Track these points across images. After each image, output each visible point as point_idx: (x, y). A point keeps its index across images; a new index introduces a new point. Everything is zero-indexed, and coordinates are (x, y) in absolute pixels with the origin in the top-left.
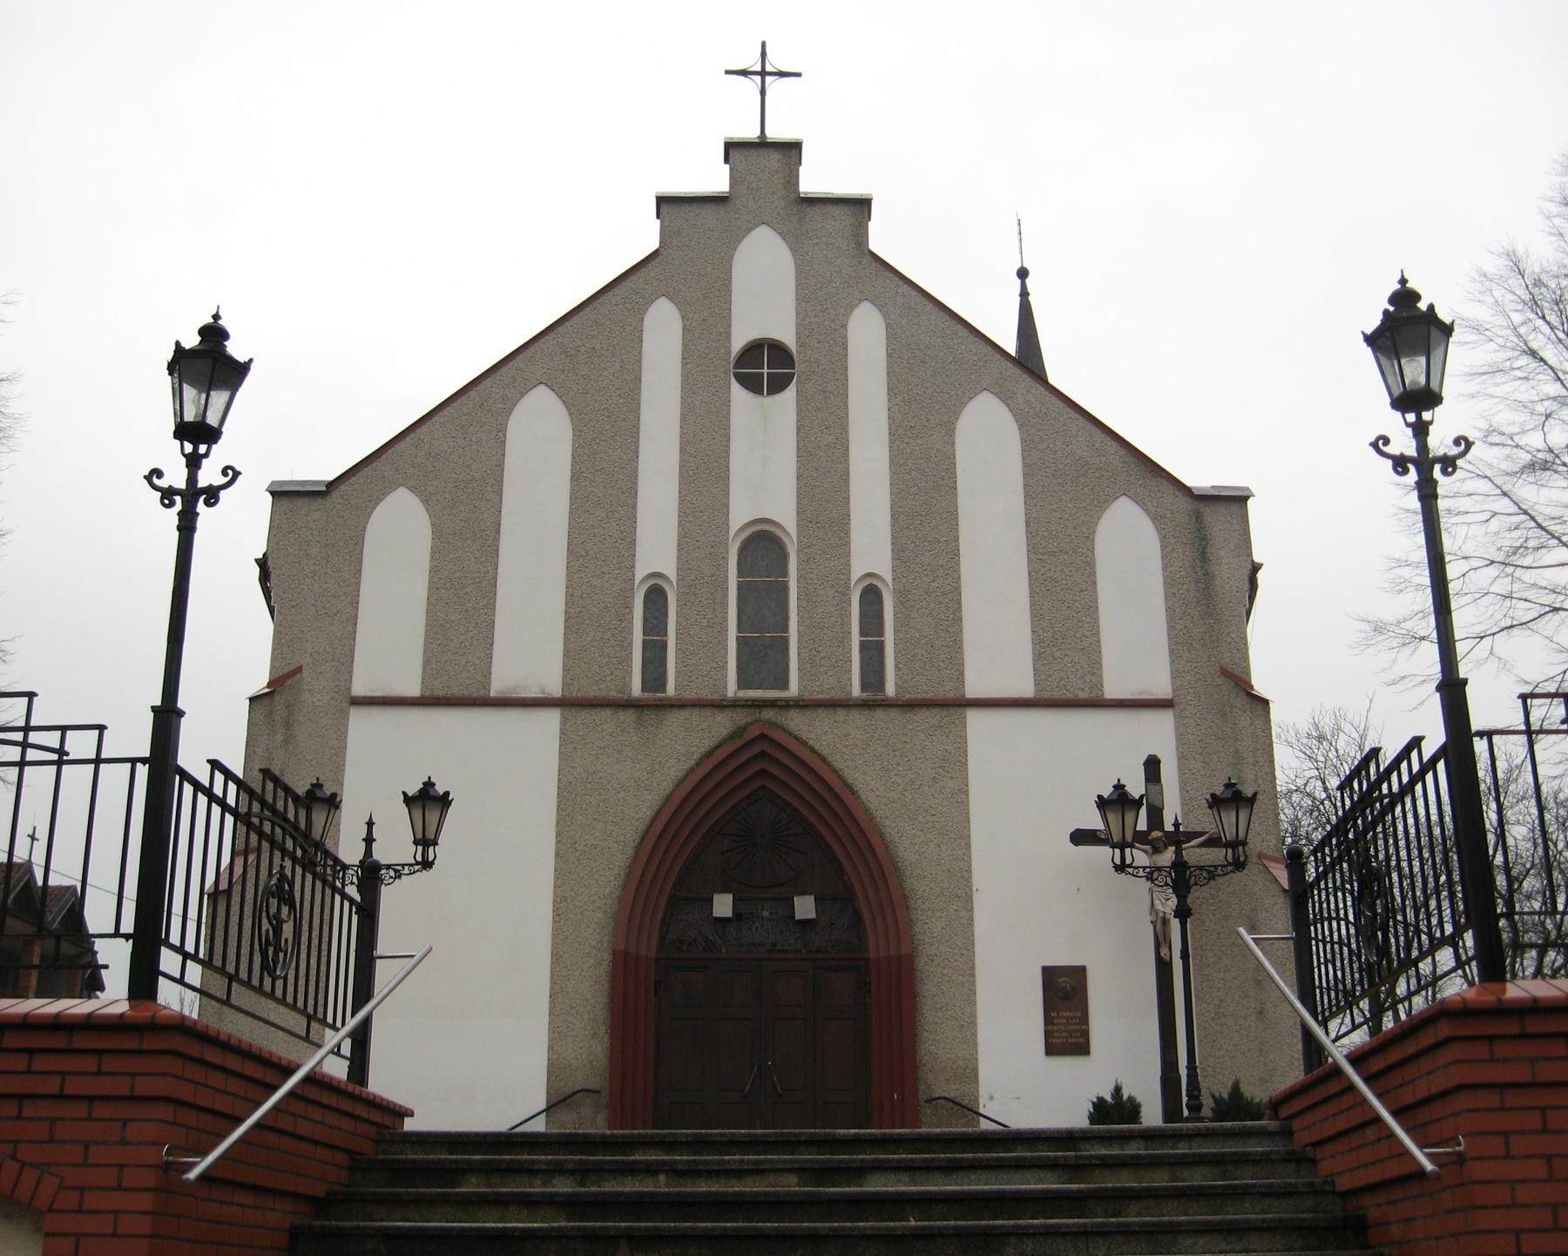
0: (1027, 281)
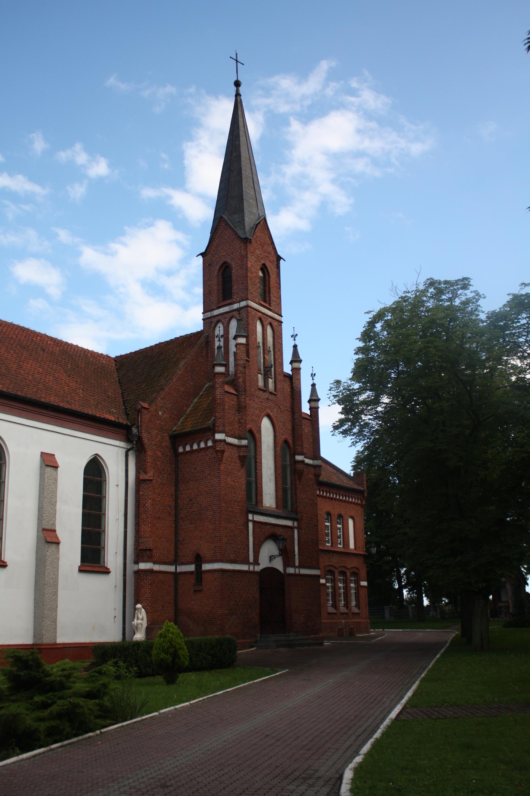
0: (241, 89)
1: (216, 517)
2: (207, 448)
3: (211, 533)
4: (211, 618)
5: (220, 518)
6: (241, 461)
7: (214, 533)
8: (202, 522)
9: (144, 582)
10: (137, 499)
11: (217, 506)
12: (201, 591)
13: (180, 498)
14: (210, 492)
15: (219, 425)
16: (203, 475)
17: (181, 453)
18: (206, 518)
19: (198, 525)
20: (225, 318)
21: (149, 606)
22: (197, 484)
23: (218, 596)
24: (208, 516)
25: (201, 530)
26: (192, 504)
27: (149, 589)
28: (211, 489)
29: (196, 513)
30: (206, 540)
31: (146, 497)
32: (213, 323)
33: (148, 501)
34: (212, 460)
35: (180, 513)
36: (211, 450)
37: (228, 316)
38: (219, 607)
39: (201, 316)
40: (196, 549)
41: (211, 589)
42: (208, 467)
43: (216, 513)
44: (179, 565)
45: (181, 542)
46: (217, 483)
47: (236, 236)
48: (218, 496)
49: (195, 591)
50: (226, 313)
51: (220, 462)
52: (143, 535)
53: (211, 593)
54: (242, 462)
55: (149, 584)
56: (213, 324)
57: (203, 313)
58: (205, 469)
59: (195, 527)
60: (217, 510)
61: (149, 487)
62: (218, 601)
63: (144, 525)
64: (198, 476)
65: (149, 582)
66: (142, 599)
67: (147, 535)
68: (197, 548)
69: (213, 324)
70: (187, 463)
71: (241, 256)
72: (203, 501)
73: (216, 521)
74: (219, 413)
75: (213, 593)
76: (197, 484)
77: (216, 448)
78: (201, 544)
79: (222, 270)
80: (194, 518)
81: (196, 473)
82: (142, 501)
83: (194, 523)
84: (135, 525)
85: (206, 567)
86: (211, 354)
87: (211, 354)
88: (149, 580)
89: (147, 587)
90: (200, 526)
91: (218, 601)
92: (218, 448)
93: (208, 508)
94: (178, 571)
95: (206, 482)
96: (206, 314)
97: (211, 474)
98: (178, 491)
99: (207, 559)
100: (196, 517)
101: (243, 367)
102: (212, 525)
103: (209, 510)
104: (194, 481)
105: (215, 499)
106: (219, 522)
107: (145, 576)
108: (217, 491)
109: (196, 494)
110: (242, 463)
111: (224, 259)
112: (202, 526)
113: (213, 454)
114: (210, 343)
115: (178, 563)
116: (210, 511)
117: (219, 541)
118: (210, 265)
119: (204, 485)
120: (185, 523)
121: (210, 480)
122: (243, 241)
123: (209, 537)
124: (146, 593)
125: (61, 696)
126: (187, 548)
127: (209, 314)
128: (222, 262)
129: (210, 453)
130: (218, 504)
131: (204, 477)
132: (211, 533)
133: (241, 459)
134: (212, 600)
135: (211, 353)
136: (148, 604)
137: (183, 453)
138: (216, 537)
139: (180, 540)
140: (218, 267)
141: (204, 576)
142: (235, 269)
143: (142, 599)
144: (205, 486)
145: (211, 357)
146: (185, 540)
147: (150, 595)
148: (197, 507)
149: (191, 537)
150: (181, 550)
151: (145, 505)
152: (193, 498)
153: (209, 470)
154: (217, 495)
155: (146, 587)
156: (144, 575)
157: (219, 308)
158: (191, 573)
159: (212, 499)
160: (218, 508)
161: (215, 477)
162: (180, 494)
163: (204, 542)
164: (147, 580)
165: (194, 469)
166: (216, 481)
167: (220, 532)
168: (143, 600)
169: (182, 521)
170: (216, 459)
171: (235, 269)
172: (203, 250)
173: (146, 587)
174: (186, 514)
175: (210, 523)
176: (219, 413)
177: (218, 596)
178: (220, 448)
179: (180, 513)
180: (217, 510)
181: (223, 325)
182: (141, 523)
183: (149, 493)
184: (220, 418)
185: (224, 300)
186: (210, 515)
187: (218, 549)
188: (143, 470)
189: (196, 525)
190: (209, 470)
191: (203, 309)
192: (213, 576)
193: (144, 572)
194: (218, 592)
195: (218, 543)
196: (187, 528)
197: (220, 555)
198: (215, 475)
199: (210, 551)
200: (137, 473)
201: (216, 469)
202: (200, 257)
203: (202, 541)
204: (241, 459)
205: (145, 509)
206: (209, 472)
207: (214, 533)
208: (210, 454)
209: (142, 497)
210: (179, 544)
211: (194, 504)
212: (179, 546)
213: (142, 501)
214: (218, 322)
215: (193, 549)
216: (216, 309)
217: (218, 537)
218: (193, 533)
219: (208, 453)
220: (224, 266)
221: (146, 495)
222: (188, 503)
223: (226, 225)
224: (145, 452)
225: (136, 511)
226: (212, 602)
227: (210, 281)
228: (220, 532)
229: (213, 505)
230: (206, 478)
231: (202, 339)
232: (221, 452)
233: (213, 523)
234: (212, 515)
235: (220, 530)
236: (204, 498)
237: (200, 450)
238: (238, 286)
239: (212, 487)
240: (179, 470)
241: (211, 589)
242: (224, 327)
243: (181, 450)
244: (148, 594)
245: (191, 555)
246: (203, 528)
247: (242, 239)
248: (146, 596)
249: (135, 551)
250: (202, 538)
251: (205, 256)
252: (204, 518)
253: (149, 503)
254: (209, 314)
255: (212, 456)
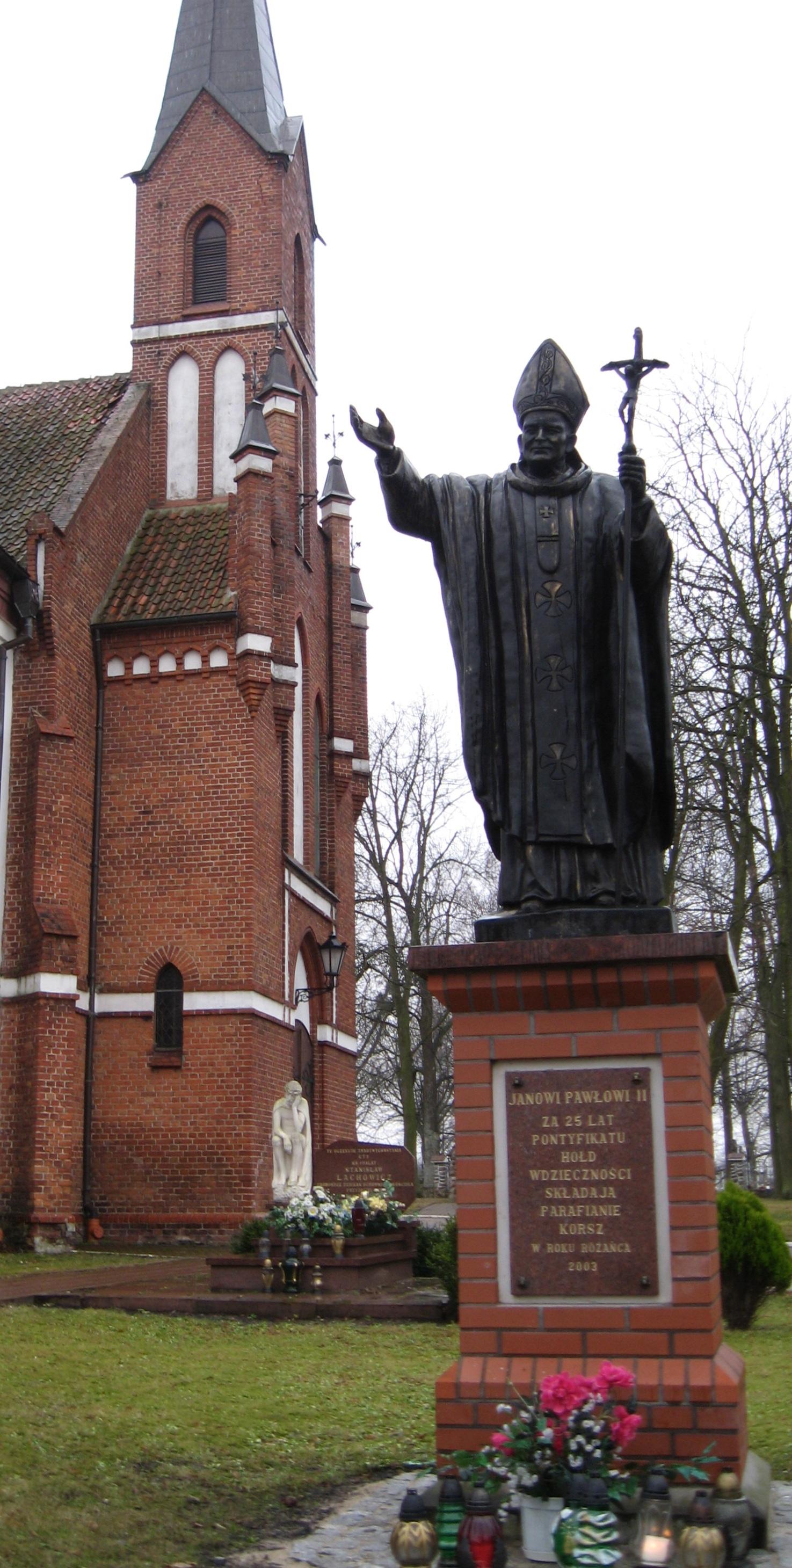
1: (236, 863)
2: (207, 673)
3: (217, 909)
4: (211, 1147)
5: (247, 868)
6: (278, 722)
7: (228, 908)
8: (186, 876)
9: (52, 1032)
10: (15, 788)
11: (239, 835)
12: (177, 1068)
13: (109, 804)
14: (214, 793)
15: (257, 613)
16: (190, 746)
17: (117, 680)
18: (200, 865)
19: (172, 882)
20: (207, 347)
21: (64, 1104)
22: (169, 769)
23: (238, 1087)
24: (207, 859)
25: (183, 899)
26: (149, 823)
27: (64, 1052)
28: (219, 787)
29: (163, 850)
30: (197, 925)
31: (53, 785)
32: (164, 355)
33: (60, 798)
34: (225, 706)
35: (108, 847)
36: (221, 680)
37: (216, 345)
38: (241, 1116)
39: (130, 335)
40: (161, 950)
41: (212, 1064)
42: (211, 723)
43: (238, 852)
44: (101, 991)
45: (109, 929)
46: (239, 770)
47: (248, 145)
48: (243, 807)
49: (155, 1068)
50: (210, 334)
51: (254, 714)
52: (43, 894)
53: (211, 1075)
54: (280, 725)
55: (64, 1039)
56: (166, 359)
57: (133, 327)
58: (197, 730)
59: (158, 888)
60: (239, 846)
61: (64, 758)
62: (238, 1099)
63: (47, 866)
64: (175, 747)
65: (64, 1032)
66: (46, 1081)
67: (52, 894)
68: (166, 948)
69: (166, 359)
70: (134, 708)
71: (262, 197)
72: (188, 816)
73: (236, 877)
74: (257, 580)
75: (220, 1076)
76: (169, 769)
77: (248, 673)
78: (179, 938)
79: (194, 227)
80: (155, 861)
81: (168, 737)
82: (42, 795)
83: (157, 878)
84: (7, 865)
85: (194, 1001)
86: (157, 436)
87: (157, 436)
88: (65, 1027)
89: (59, 1045)
90: (176, 888)
91: (238, 1099)
92: (253, 673)
93: (208, 837)
94: (97, 1009)
95: (201, 766)
96: (144, 329)
97: (220, 744)
98: (102, 783)
99: (199, 979)
100: (163, 861)
101: (287, 473)
102: (219, 885)
103: (210, 842)
104: (161, 759)
105: (231, 814)
106: (247, 879)
107: (56, 1014)
108: (240, 791)
109: (166, 796)
110: (279, 728)
111: (207, 199)
112: (183, 888)
113: (230, 690)
114: (156, 405)
115: (99, 986)
116: (215, 848)
117: (242, 930)
118: (160, 205)
119: (195, 772)
120: (124, 876)
121: (213, 760)
122: (269, 160)
123: (208, 920)
124: (56, 1064)
125: (434, 1412)
126: (130, 946)
127: (153, 332)
128: (199, 203)
129: (218, 685)
130: (243, 829)
131: (197, 751)
132: (217, 909)
133: (279, 717)
134: (215, 1097)
135: (155, 431)
136: (60, 1098)
137: (123, 680)
138: (236, 919)
139: (106, 923)
140: (185, 216)
141: (187, 1026)
142: (241, 227)
143: (46, 1081)
144: (199, 777)
145: (157, 444)
146: (123, 923)
147: (68, 1071)
148: (167, 834)
149: (145, 916)
150: (108, 951)
151: (49, 809)
152: (154, 807)
153: (212, 734)
154: (239, 802)
155: (56, 1047)
156: (52, 1009)
157: (187, 318)
158: (145, 1016)
159: (222, 814)
160: (243, 840)
161: (235, 754)
162: (108, 793)
163: (192, 931)
164: (58, 1027)
165: (159, 727)
166: (236, 764)
167: (249, 907)
168: (49, 1084)
169: (112, 870)
170: (239, 705)
171: (241, 227)
172: (138, 167)
173: (56, 1047)
174: (129, 851)
175: (215, 880)
176: (257, 580)
177: (238, 1087)
178: (258, 674)
179: (108, 847)
180: (239, 846)
181: (199, 364)
182: (40, 859)
183: (61, 775)
184: (259, 594)
185: (195, 302)
186: (213, 859)
187: (241, 953)
188: (40, 709)
189: (161, 883)
190: (212, 734)
191: (135, 315)
192: (221, 1029)
193: (52, 1003)
194: (237, 1075)
195: (238, 936)
196: (132, 890)
197: (246, 970)
198: (233, 748)
199: (214, 959)
200: (20, 715)
201: (237, 732)
202: (129, 179)
203: (184, 929)
204: (279, 717)
205: (49, 819)
206: (214, 739)
207: (228, 908)
208: (219, 691)
209: (43, 784)
210: (100, 934)
211: (160, 823)
212: (101, 940)
213: (42, 795)
214: (183, 353)
215: (153, 949)
216: (177, 321)
217: (242, 919)
218: (152, 906)
219: (210, 686)
220: (206, 214)
221: (54, 779)
222: (136, 818)
223: (216, 112)
224: (52, 656)
225: (14, 823)
226: (216, 1102)
227: (160, 246)
228: (249, 907)
229: (226, 830)
230: (202, 753)
231: (131, 396)
232: (259, 686)
233: (224, 880)
234: (222, 858)
235: (247, 901)
236: (193, 810)
237: (182, 676)
238: (248, 272)
239: (222, 782)
240: (109, 725)
241: (212, 1064)
242: (200, 371)
243: (115, 669)
244: (60, 1067)
245: (145, 967)
246: (187, 893)
247: (265, 152)
248: (56, 1073)
249: (6, 941)
250: (185, 921)
251: (146, 181)
252: (194, 865)
253: (62, 803)
254: (153, 332)
255: (223, 695)
